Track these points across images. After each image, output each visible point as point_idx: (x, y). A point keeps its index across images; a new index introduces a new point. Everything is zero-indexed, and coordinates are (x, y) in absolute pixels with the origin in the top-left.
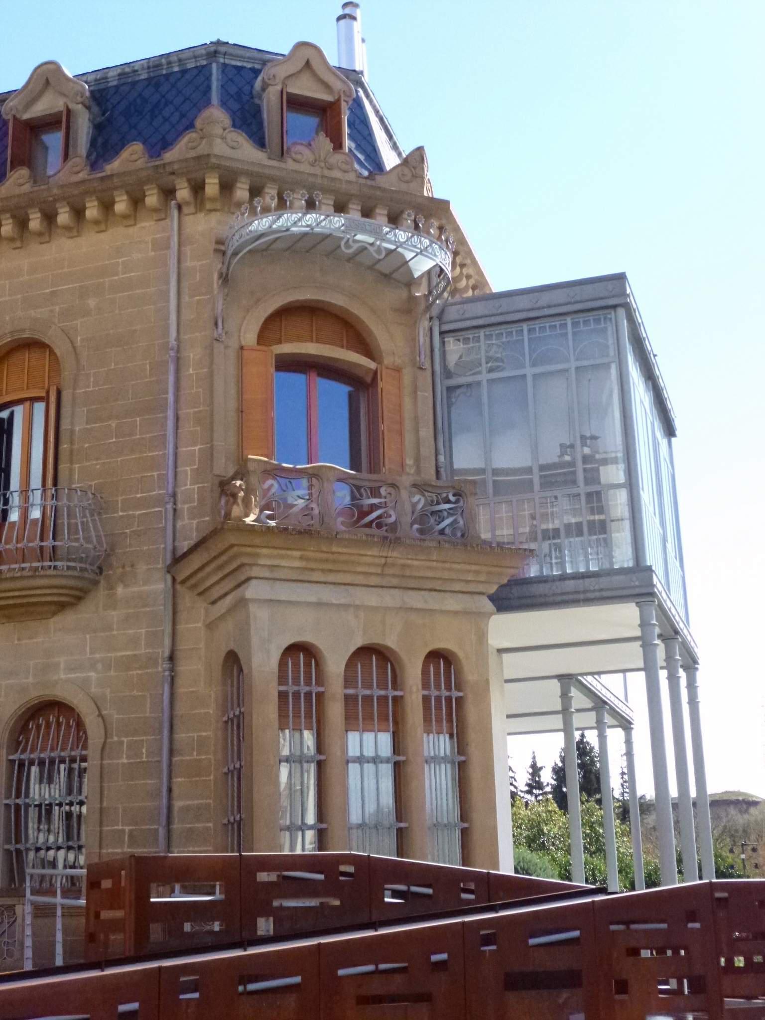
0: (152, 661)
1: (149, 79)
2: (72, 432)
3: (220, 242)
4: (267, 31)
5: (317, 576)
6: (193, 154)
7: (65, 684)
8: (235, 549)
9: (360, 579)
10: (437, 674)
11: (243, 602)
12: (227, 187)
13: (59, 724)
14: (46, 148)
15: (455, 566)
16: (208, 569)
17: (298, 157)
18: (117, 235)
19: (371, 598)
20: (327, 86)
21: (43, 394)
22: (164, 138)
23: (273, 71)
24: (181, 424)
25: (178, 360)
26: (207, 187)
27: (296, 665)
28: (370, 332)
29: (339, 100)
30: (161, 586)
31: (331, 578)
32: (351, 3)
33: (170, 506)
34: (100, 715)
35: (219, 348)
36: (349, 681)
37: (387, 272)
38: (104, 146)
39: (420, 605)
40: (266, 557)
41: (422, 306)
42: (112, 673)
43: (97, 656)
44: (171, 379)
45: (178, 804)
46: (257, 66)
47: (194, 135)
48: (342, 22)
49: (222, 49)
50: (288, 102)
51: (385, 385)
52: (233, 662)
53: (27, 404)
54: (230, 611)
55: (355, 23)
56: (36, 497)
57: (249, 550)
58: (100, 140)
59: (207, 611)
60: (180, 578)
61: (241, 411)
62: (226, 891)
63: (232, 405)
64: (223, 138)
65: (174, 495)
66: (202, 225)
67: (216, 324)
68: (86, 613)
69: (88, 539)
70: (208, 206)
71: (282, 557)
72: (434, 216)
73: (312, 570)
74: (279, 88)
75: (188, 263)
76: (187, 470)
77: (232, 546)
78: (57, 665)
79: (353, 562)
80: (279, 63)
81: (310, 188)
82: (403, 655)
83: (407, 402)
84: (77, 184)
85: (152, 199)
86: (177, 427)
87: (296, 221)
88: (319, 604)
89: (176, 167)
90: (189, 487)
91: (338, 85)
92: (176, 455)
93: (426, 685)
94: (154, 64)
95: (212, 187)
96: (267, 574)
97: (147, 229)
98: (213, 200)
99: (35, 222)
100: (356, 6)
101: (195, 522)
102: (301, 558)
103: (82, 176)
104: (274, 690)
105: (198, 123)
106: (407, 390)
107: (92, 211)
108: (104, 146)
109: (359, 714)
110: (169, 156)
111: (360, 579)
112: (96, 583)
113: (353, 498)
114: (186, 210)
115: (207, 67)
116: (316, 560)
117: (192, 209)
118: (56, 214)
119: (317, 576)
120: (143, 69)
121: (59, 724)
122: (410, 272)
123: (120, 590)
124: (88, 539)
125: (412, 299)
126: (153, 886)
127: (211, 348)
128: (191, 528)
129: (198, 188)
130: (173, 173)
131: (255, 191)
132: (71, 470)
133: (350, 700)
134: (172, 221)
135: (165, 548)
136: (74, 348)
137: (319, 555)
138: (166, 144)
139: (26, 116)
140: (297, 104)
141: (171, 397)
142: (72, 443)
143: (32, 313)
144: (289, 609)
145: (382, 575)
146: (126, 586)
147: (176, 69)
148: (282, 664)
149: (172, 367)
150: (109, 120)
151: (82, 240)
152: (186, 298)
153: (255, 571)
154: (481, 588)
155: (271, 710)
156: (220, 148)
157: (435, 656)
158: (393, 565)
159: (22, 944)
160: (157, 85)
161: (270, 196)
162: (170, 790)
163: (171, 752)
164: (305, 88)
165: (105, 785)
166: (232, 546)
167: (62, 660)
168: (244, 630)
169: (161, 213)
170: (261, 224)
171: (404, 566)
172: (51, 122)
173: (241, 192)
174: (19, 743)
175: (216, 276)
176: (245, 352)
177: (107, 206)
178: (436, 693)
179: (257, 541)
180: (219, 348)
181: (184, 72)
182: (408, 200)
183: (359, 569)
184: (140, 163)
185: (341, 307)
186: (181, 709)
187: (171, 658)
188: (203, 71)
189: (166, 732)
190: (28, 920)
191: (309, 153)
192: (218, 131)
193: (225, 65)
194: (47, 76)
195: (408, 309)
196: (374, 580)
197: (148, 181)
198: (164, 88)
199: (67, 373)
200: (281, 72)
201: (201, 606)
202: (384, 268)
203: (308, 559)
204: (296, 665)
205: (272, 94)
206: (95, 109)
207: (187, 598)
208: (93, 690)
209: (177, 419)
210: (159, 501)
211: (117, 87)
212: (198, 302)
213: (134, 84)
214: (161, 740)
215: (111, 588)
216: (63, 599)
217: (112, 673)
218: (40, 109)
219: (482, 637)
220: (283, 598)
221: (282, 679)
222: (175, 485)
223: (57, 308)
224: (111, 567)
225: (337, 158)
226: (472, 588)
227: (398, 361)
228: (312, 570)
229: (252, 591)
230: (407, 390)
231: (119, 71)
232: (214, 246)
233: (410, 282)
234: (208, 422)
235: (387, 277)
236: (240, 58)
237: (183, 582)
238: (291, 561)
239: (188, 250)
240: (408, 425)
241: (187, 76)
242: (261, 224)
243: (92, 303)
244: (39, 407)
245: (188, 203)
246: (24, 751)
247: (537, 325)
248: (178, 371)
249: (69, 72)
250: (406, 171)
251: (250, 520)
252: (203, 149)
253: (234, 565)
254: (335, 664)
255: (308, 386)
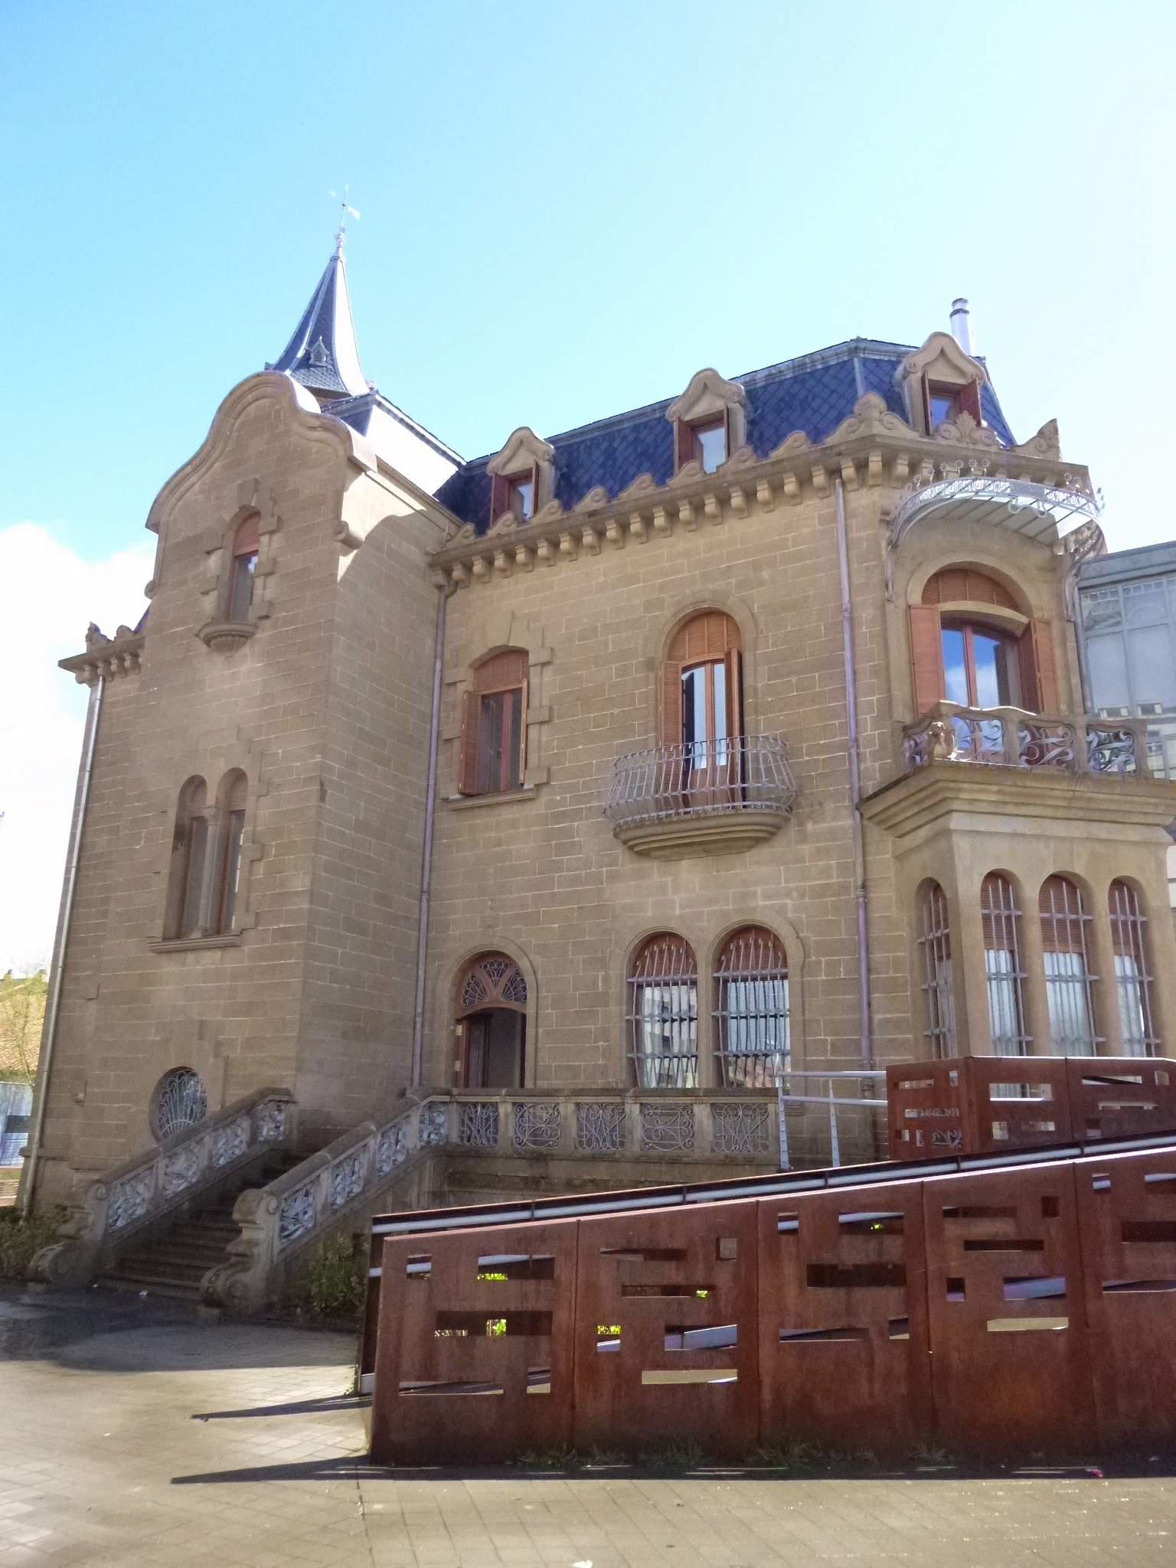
0: (844, 888)
1: (795, 378)
2: (756, 690)
3: (886, 513)
4: (905, 324)
5: (1009, 809)
6: (853, 437)
7: (762, 909)
8: (940, 784)
9: (1049, 812)
10: (1122, 900)
11: (947, 833)
12: (888, 464)
13: (757, 946)
14: (522, 497)
15: (1136, 799)
16: (903, 804)
17: (945, 434)
18: (783, 514)
19: (1060, 829)
20: (962, 373)
21: (722, 656)
22: (816, 428)
23: (913, 360)
24: (858, 677)
25: (852, 620)
26: (871, 465)
27: (996, 890)
28: (1019, 590)
29: (973, 382)
30: (849, 822)
31: (1023, 810)
32: (961, 299)
33: (853, 751)
34: (798, 937)
35: (890, 607)
36: (1044, 905)
37: (1031, 534)
38: (568, 490)
39: (1104, 835)
40: (968, 792)
41: (1068, 562)
42: (807, 900)
43: (791, 885)
44: (847, 637)
45: (877, 1017)
46: (893, 359)
47: (853, 420)
48: (956, 317)
49: (862, 345)
50: (931, 389)
51: (1039, 636)
52: (932, 889)
53: (709, 666)
54: (927, 842)
55: (968, 317)
56: (722, 747)
57: (952, 785)
58: (756, 434)
59: (894, 843)
60: (868, 815)
61: (912, 664)
62: (1056, 1092)
63: (905, 658)
64: (880, 421)
65: (857, 740)
66: (866, 500)
67: (887, 586)
68: (778, 847)
69: (783, 782)
70: (871, 482)
71: (982, 791)
72: (1072, 478)
73: (1005, 803)
74: (920, 374)
75: (855, 535)
76: (867, 718)
77: (937, 781)
78: (755, 894)
79: (1043, 796)
80: (916, 354)
81: (966, 459)
82: (1091, 883)
83: (1058, 652)
84: (748, 470)
85: (819, 479)
86: (855, 680)
87: (956, 489)
88: (1014, 835)
89: (843, 448)
90: (870, 732)
91: (970, 370)
92: (856, 704)
93: (1113, 911)
94: (799, 365)
95: (875, 464)
96: (966, 807)
97: (812, 508)
98: (875, 476)
99: (711, 507)
100: (966, 301)
101: (877, 765)
102: (999, 792)
103: (748, 464)
104: (978, 912)
105: (857, 409)
106: (1056, 643)
107: (763, 493)
108: (568, 490)
109: (1056, 936)
110: (830, 440)
111: (1049, 812)
112: (787, 820)
113: (1034, 737)
114: (849, 487)
115: (851, 360)
116: (1010, 794)
117: (855, 486)
118: (729, 498)
119: (1009, 809)
120: (788, 369)
121: (757, 946)
122: (1056, 532)
123: (810, 826)
124: (783, 782)
125: (1054, 557)
126: (993, 1086)
127: (883, 606)
128: (874, 771)
129: (862, 466)
130: (840, 454)
131: (914, 468)
132: (757, 722)
133: (1046, 924)
134: (837, 498)
135: (851, 789)
136: (753, 614)
137: (1014, 789)
138: (623, 484)
139: (687, 418)
140: (940, 390)
141: (847, 654)
142: (756, 696)
143: (711, 586)
144: (985, 841)
145: (1069, 808)
146: (815, 822)
147: (819, 367)
148: (984, 890)
149: (847, 625)
150: (762, 417)
151: (726, 527)
152: (855, 566)
153: (956, 805)
154: (1158, 820)
155: (978, 932)
156: (877, 429)
157: (1118, 884)
158: (1081, 798)
159: (777, 1139)
160: (803, 382)
161: (927, 470)
162: (869, 1005)
163: (869, 971)
164: (941, 374)
165: (807, 999)
166: (937, 781)
167: (759, 890)
168: (947, 859)
169: (824, 491)
170: (928, 494)
171: (1089, 799)
172: (523, 477)
173: (902, 468)
174: (635, 967)
175: (884, 544)
176: (913, 611)
177: (777, 488)
178: (1132, 918)
179: (960, 777)
180: (890, 607)
181: (827, 369)
182: (1045, 465)
183: (1049, 802)
184: (804, 448)
185: (992, 568)
186: (875, 932)
187: (864, 886)
188: (845, 366)
189: (863, 954)
190: (782, 1118)
191: (954, 432)
192: (876, 414)
193: (865, 360)
194: (522, 439)
195: (1054, 567)
196: (1060, 813)
197: (816, 463)
198: (811, 382)
199: (748, 637)
200: (921, 360)
201: (889, 841)
202: (1031, 530)
203: (1004, 793)
204: (996, 890)
205: (915, 378)
206: (750, 407)
207: (875, 833)
208: (790, 915)
209: (855, 673)
210: (843, 746)
211: (765, 387)
212: (867, 568)
213: (781, 382)
214: (859, 959)
215: (801, 824)
216: (760, 835)
217: (807, 900)
218: (513, 467)
219: (1161, 865)
220: (982, 829)
221: (985, 904)
222: (857, 732)
223: (734, 581)
224: (799, 806)
225: (978, 434)
226: (1150, 820)
227: (1046, 615)
228: (1005, 803)
229: (956, 822)
230: (1056, 643)
231: (766, 373)
232: (879, 516)
233: (1053, 541)
234: (884, 672)
235: (1031, 539)
236: (880, 352)
237: (870, 818)
238: (989, 795)
239: (853, 522)
240: (1060, 673)
241: (831, 372)
242: (928, 494)
243: (765, 574)
244: (720, 670)
245: (851, 481)
246: (641, 974)
247: (1131, 585)
248: (852, 630)
249: (726, 374)
250: (1042, 441)
251: (953, 757)
252: (863, 431)
253: (937, 799)
254: (1031, 890)
255: (965, 640)
